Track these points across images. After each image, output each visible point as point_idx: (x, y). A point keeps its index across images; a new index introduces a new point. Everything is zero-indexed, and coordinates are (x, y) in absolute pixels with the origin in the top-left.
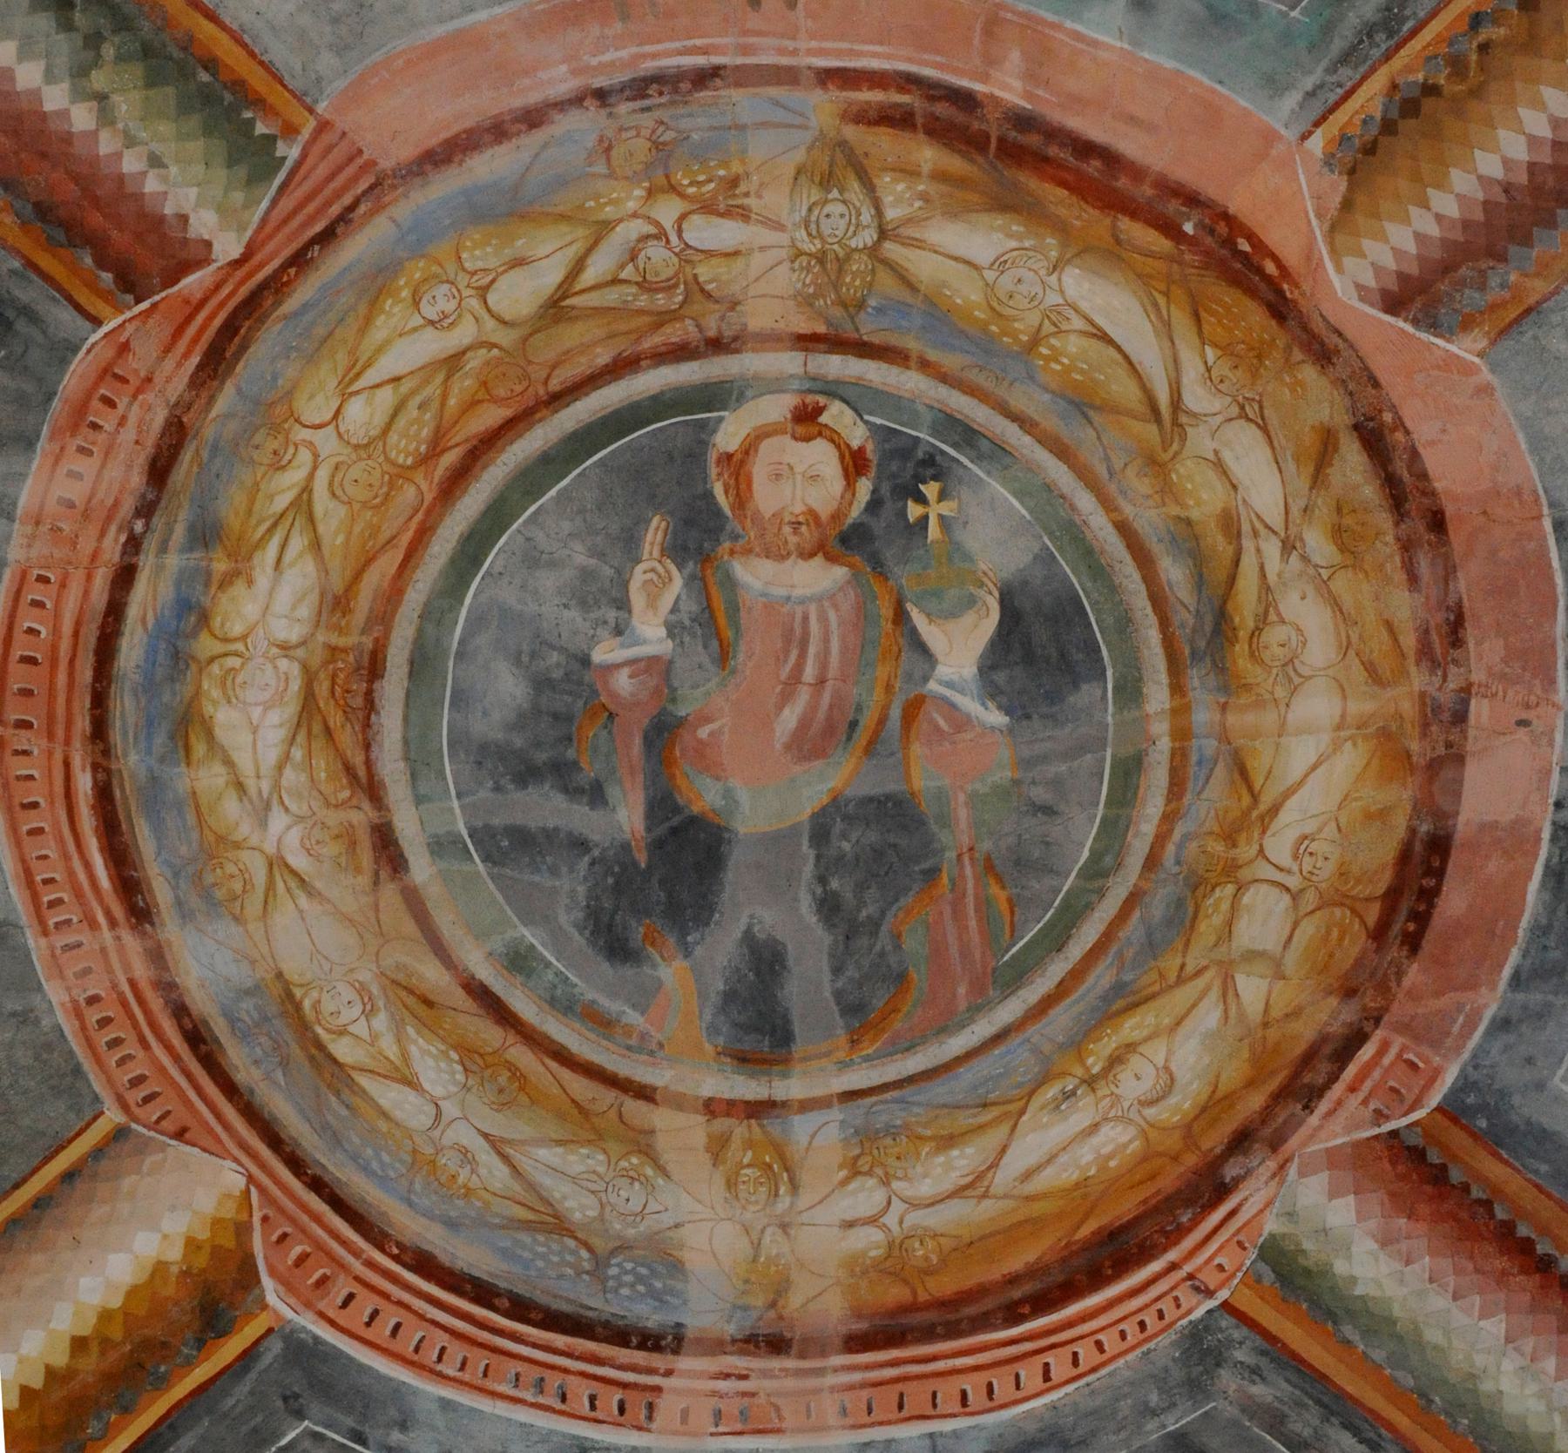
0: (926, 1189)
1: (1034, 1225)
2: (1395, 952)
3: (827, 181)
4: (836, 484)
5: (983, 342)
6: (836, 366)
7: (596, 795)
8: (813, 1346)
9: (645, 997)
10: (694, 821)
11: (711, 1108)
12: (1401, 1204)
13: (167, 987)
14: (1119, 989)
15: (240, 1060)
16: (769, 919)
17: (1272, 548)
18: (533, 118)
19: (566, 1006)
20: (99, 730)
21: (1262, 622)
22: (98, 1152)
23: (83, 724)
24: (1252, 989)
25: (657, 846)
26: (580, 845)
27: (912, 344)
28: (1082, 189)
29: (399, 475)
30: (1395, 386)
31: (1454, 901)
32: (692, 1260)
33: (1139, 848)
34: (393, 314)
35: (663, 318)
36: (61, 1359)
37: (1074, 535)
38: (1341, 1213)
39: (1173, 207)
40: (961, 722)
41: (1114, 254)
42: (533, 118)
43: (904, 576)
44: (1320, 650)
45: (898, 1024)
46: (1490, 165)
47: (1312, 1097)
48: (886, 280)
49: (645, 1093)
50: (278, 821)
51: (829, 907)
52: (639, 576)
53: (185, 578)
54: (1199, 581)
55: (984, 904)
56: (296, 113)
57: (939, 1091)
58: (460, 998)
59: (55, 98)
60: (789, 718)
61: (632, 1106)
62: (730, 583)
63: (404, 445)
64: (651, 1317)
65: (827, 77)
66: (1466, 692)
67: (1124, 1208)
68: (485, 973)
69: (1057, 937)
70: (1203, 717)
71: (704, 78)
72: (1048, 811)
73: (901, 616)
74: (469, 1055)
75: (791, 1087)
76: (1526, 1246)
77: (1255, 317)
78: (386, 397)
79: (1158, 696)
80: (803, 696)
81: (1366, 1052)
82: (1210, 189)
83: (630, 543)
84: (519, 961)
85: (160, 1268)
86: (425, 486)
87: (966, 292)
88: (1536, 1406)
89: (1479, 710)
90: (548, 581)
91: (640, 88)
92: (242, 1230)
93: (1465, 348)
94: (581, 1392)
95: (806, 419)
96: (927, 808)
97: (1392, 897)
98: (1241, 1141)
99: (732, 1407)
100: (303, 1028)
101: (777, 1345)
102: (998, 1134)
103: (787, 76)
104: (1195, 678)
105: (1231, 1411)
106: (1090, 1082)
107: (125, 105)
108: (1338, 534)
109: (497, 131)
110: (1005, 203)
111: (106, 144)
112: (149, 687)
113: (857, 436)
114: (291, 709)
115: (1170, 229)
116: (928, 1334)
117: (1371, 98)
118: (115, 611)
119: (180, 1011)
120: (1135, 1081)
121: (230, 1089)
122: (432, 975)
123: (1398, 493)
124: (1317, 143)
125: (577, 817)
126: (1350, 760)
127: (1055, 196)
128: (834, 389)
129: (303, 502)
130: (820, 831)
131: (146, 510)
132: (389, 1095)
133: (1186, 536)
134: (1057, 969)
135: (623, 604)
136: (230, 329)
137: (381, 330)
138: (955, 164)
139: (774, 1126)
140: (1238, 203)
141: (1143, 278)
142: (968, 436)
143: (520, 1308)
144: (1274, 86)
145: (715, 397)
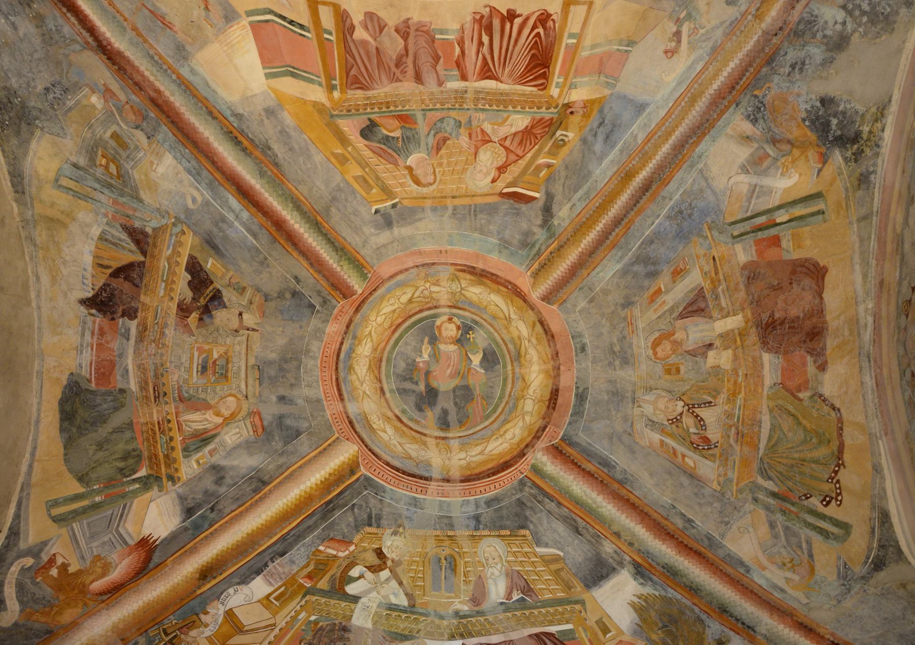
0: (473, 454)
1: (492, 460)
2: (551, 410)
3: (453, 280)
4: (455, 332)
5: (478, 307)
6: (455, 311)
7: (417, 383)
8: (454, 481)
9: (425, 418)
10: (433, 388)
11: (436, 438)
12: (555, 457)
13: (346, 413)
14: (505, 420)
15: (357, 426)
16: (446, 406)
17: (527, 342)
18: (407, 270)
19: (411, 420)
20: (337, 369)
21: (526, 354)
22: (334, 441)
23: (334, 367)
24: (527, 418)
25: (427, 392)
26: (414, 391)
27: (467, 308)
28: (493, 281)
29: (385, 330)
30: (544, 314)
31: (560, 401)
32: (434, 465)
33: (507, 393)
34: (385, 303)
35: (427, 303)
36: (327, 476)
37: (494, 340)
38: (545, 459)
39: (507, 284)
40: (477, 372)
41: (498, 292)
42: (407, 270)
43: (467, 347)
44: (535, 359)
45: (468, 425)
46: (555, 275)
47: (538, 438)
48: (463, 298)
49: (425, 435)
50: (365, 385)
51: (456, 404)
52: (424, 347)
53: (351, 344)
54: (515, 348)
55: (482, 404)
56: (370, 269)
57: (475, 436)
58: (394, 418)
59: (335, 266)
60: (449, 371)
61: (423, 438)
62: (439, 348)
63: (386, 325)
64: (427, 475)
65: (452, 264)
66: (560, 365)
67: (507, 458)
68: (398, 413)
69: (494, 411)
70: (517, 370)
71: (433, 264)
72: (492, 387)
73: (467, 354)
74: (396, 429)
75: (450, 435)
76: (576, 464)
77: (521, 302)
78: (384, 317)
79: (509, 367)
80: (451, 368)
81: (547, 429)
82: (513, 281)
83: (422, 342)
84: (404, 412)
85: (344, 462)
86: (390, 332)
87: (475, 298)
88: (579, 491)
89: (562, 368)
90: (409, 348)
91: (423, 265)
92: (357, 457)
93: (554, 307)
94: (414, 488)
95: (450, 319)
96: (471, 387)
97: (550, 400)
98: (527, 446)
99: (440, 492)
100: (368, 421)
101: (448, 481)
102: (485, 444)
103: (446, 264)
104: (515, 364)
105: (527, 494)
106: (501, 436)
107: (345, 268)
108: (537, 339)
109: (401, 272)
110: (481, 283)
111: (342, 273)
112: (345, 362)
113: (459, 323)
114: (367, 367)
115: (506, 287)
116: (474, 480)
117: (536, 266)
118: (340, 349)
119: (348, 417)
120: (509, 436)
121: (356, 432)
122: (390, 414)
123: (546, 332)
124: (529, 273)
125: (414, 387)
126: (541, 377)
127: (488, 282)
128: (454, 315)
129: (370, 333)
130: (454, 390)
131: (345, 333)
132: (382, 434)
133: (512, 340)
134: (495, 416)
135: (421, 352)
136: (359, 305)
137: (383, 305)
138: (472, 278)
139: (447, 441)
140: (517, 283)
141: (503, 296)
142: (476, 323)
143: (404, 473)
144: (521, 264)
145: (435, 316)
